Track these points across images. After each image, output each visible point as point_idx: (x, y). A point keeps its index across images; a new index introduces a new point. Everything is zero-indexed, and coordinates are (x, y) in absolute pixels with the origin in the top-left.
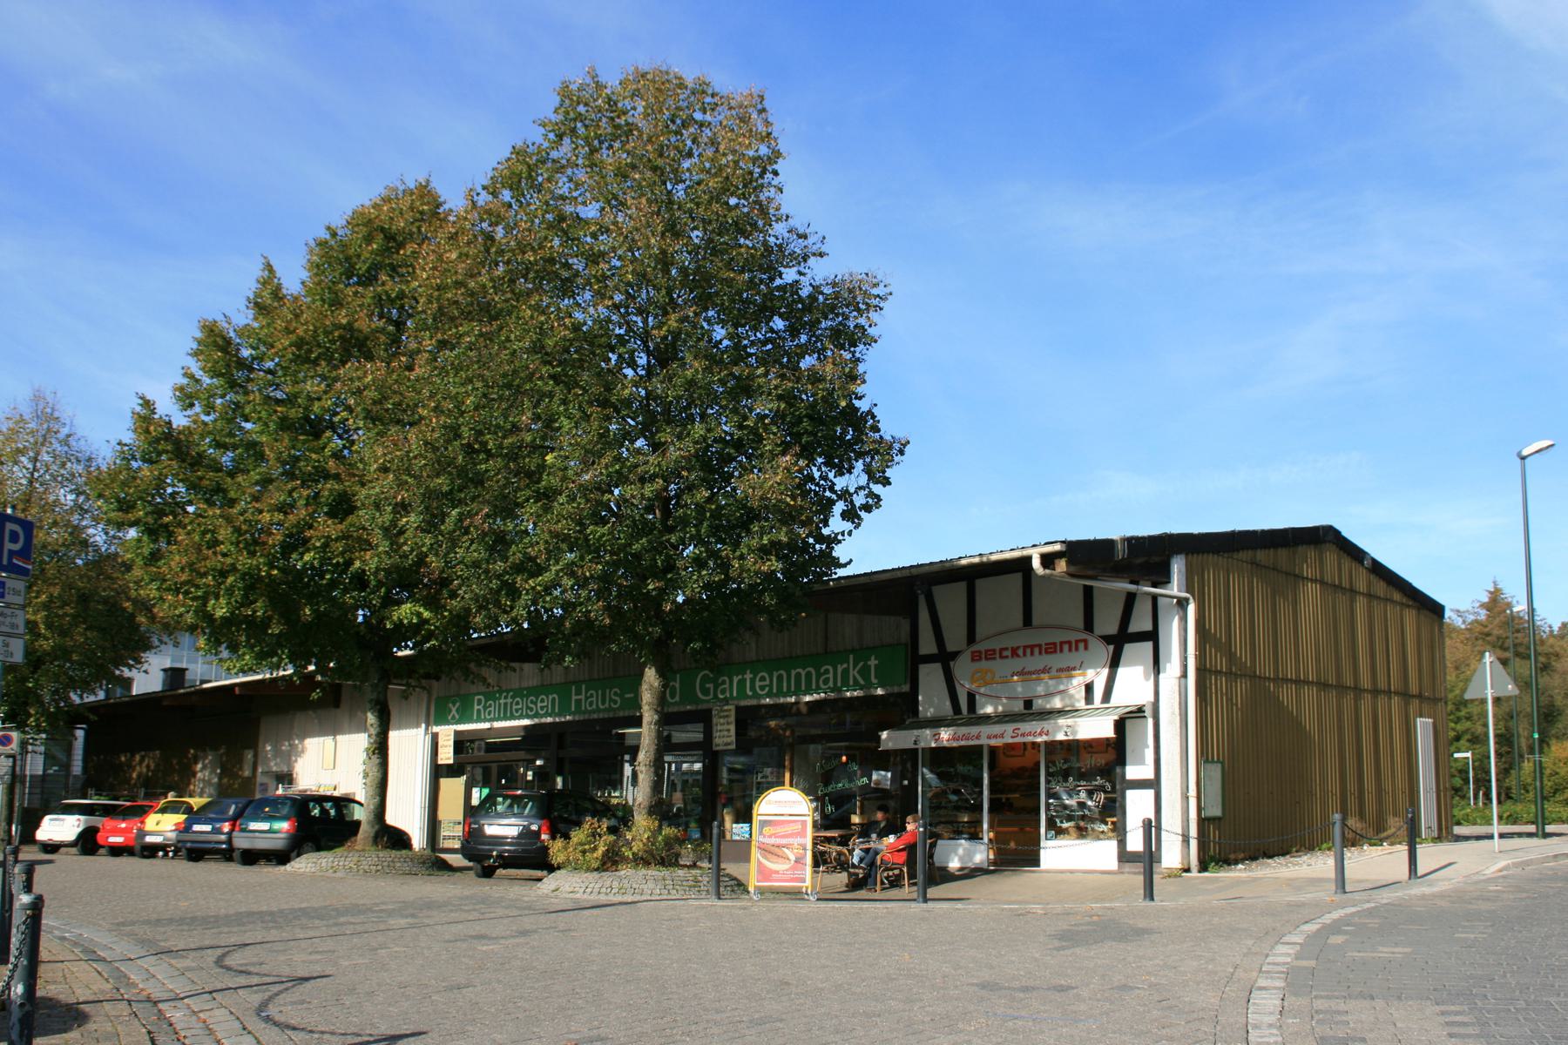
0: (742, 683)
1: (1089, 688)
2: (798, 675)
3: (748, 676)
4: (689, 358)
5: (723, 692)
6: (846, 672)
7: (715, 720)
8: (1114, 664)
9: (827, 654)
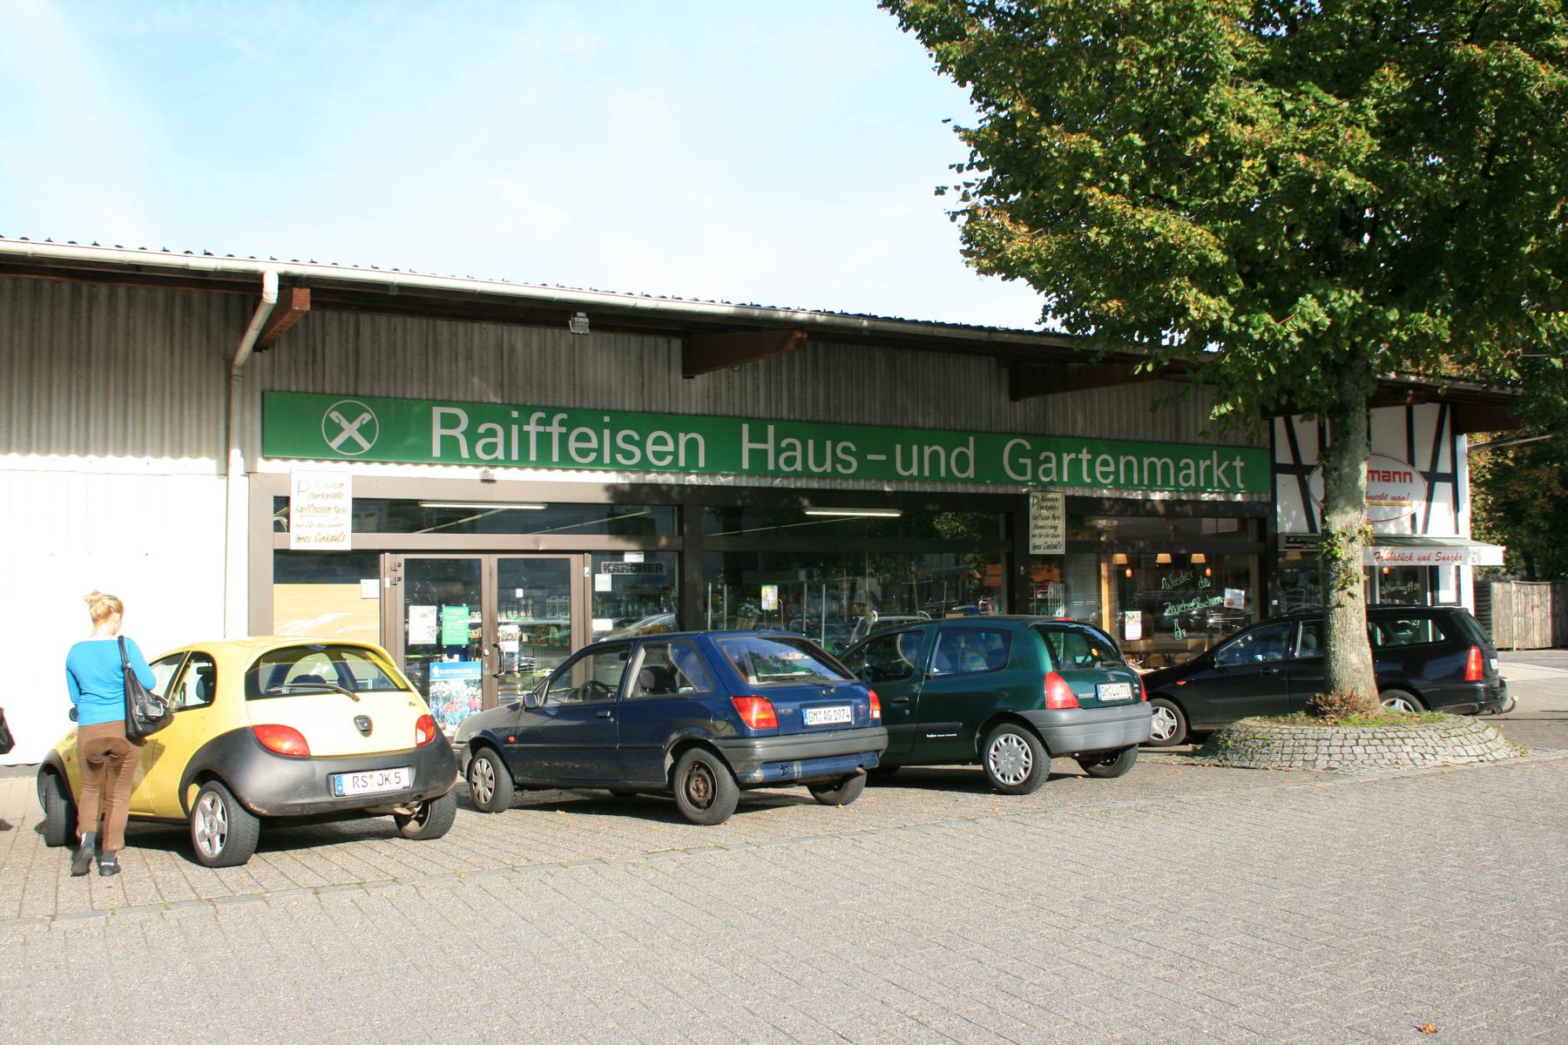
0: (1075, 464)
1: (1413, 517)
2: (1152, 466)
3: (1085, 456)
4: (1089, 192)
5: (1047, 473)
6: (1209, 469)
7: (1033, 511)
8: (1429, 499)
9: (1178, 448)
